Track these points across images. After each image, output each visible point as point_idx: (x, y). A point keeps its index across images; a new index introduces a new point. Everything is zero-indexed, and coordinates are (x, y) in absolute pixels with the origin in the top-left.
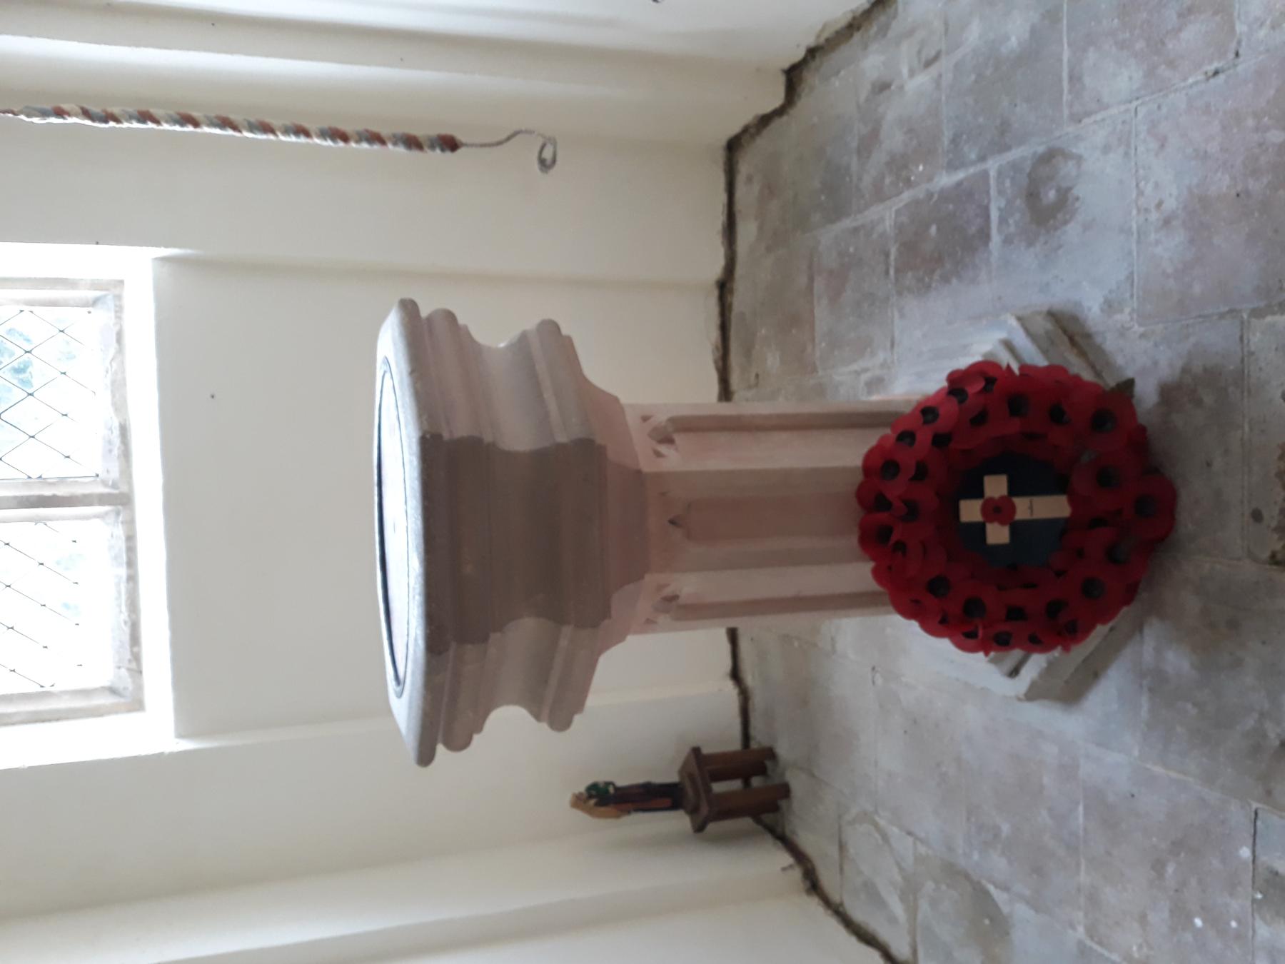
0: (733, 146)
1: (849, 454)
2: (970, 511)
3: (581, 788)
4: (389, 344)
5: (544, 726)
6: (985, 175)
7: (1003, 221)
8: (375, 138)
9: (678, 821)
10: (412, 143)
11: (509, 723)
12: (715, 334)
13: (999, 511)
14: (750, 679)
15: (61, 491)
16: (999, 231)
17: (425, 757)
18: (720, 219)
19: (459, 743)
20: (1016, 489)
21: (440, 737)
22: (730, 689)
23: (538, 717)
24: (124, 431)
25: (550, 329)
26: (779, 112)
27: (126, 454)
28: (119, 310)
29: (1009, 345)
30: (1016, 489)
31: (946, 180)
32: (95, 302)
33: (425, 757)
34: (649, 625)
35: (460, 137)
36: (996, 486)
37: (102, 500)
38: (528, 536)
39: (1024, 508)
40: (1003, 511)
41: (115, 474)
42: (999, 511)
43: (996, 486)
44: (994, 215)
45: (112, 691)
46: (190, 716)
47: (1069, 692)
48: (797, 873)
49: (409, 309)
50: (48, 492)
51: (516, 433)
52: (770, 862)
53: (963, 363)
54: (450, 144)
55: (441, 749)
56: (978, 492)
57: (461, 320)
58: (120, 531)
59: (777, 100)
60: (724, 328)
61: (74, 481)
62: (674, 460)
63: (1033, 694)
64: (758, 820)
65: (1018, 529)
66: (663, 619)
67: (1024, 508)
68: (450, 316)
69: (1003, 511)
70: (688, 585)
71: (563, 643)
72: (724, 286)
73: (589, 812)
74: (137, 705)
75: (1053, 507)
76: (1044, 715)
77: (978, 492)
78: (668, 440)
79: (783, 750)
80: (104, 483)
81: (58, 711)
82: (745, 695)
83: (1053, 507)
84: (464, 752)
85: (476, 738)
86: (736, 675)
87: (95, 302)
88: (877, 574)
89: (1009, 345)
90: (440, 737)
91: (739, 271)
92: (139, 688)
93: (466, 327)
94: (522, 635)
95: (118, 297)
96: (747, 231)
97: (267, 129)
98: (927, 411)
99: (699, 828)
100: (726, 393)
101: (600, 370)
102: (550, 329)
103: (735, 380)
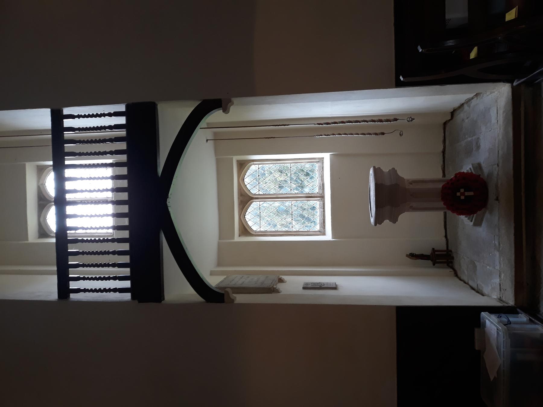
0: (445, 124)
1: (440, 186)
2: (458, 194)
3: (408, 254)
4: (371, 172)
8: (370, 134)
9: (430, 262)
10: (376, 134)
12: (442, 163)
13: (463, 194)
14: (448, 237)
15: (312, 195)
18: (442, 139)
20: (465, 191)
22: (444, 239)
24: (323, 185)
25: (393, 169)
26: (450, 120)
27: (323, 189)
28: (323, 163)
29: (470, 169)
30: (465, 191)
31: (469, 139)
32: (318, 162)
34: (408, 211)
35: (385, 132)
36: (462, 190)
37: (319, 197)
38: (392, 197)
39: (467, 194)
40: (462, 194)
41: (321, 192)
42: (463, 194)
43: (462, 190)
45: (320, 232)
46: (334, 235)
47: (478, 224)
48: (453, 273)
49: (374, 167)
51: (387, 183)
52: (449, 270)
53: (457, 172)
54: (383, 134)
56: (459, 191)
58: (322, 203)
59: (449, 118)
60: (444, 161)
61: (314, 193)
64: (448, 265)
65: (466, 197)
67: (467, 194)
68: (380, 168)
69: (462, 194)
72: (444, 152)
73: (410, 258)
74: (324, 234)
75: (471, 193)
77: (459, 191)
78: (411, 184)
79: (453, 251)
82: (447, 240)
83: (471, 193)
86: (446, 236)
87: (318, 162)
88: (444, 204)
89: (470, 169)
91: (446, 149)
92: (325, 231)
95: (323, 161)
97: (352, 134)
98: (451, 179)
99: (434, 265)
100: (444, 175)
101: (400, 173)
102: (393, 169)
103: (446, 174)
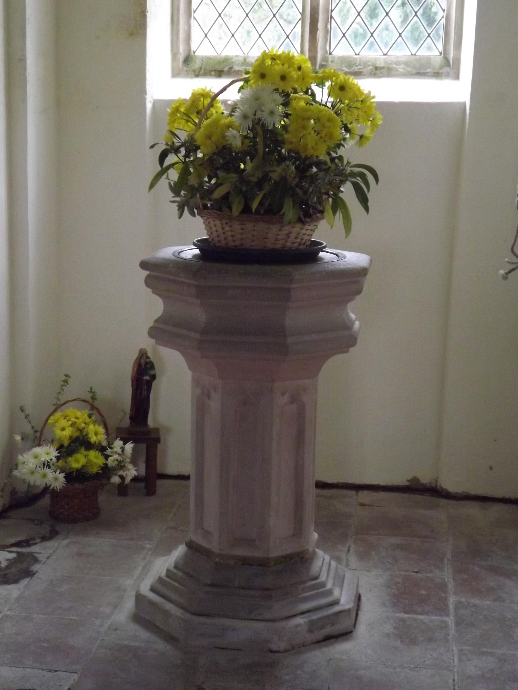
5: (151, 324)
6: (448, 615)
7: (416, 620)
11: (155, 307)
15: (320, 34)
16: (409, 618)
17: (144, 265)
19: (149, 282)
21: (152, 273)
23: (157, 321)
33: (144, 265)
34: (196, 382)
44: (421, 617)
50: (320, 25)
55: (146, 273)
57: (358, 298)
62: (283, 400)
63: (139, 598)
66: (198, 391)
70: (215, 405)
71: (192, 334)
72: (434, 492)
76: (129, 605)
80: (325, 59)
81: (178, 24)
84: (145, 285)
85: (150, 290)
90: (152, 273)
93: (354, 299)
94: (198, 313)
96: (473, 510)
